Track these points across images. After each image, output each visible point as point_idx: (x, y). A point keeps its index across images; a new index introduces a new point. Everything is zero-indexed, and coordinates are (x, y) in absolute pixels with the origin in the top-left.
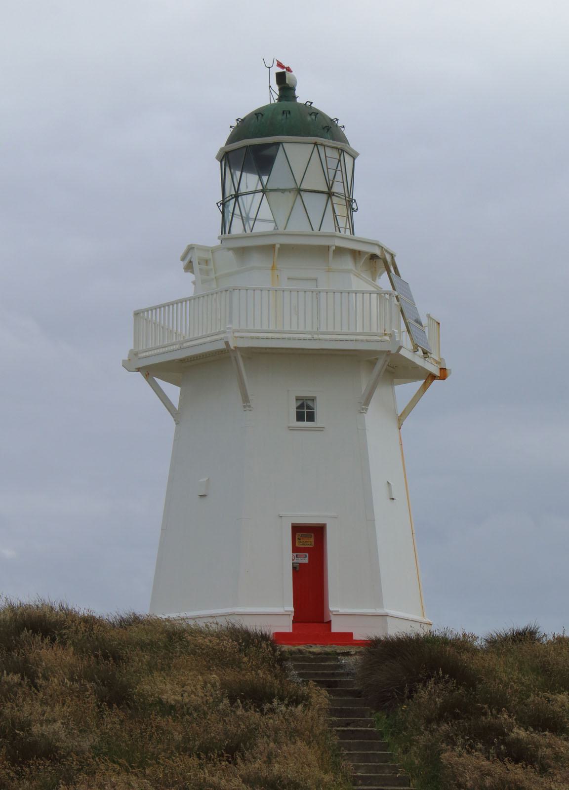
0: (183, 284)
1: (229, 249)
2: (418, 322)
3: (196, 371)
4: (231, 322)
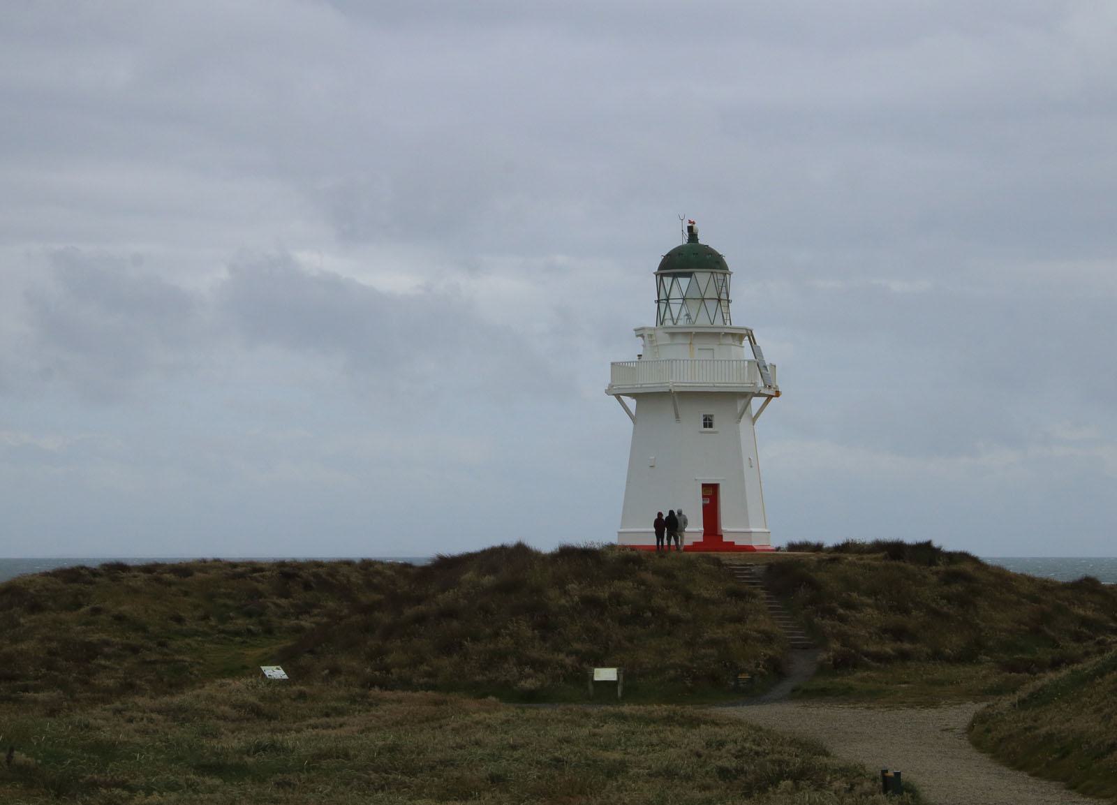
0: (638, 346)
1: (667, 333)
2: (765, 367)
3: (650, 400)
4: (672, 377)
